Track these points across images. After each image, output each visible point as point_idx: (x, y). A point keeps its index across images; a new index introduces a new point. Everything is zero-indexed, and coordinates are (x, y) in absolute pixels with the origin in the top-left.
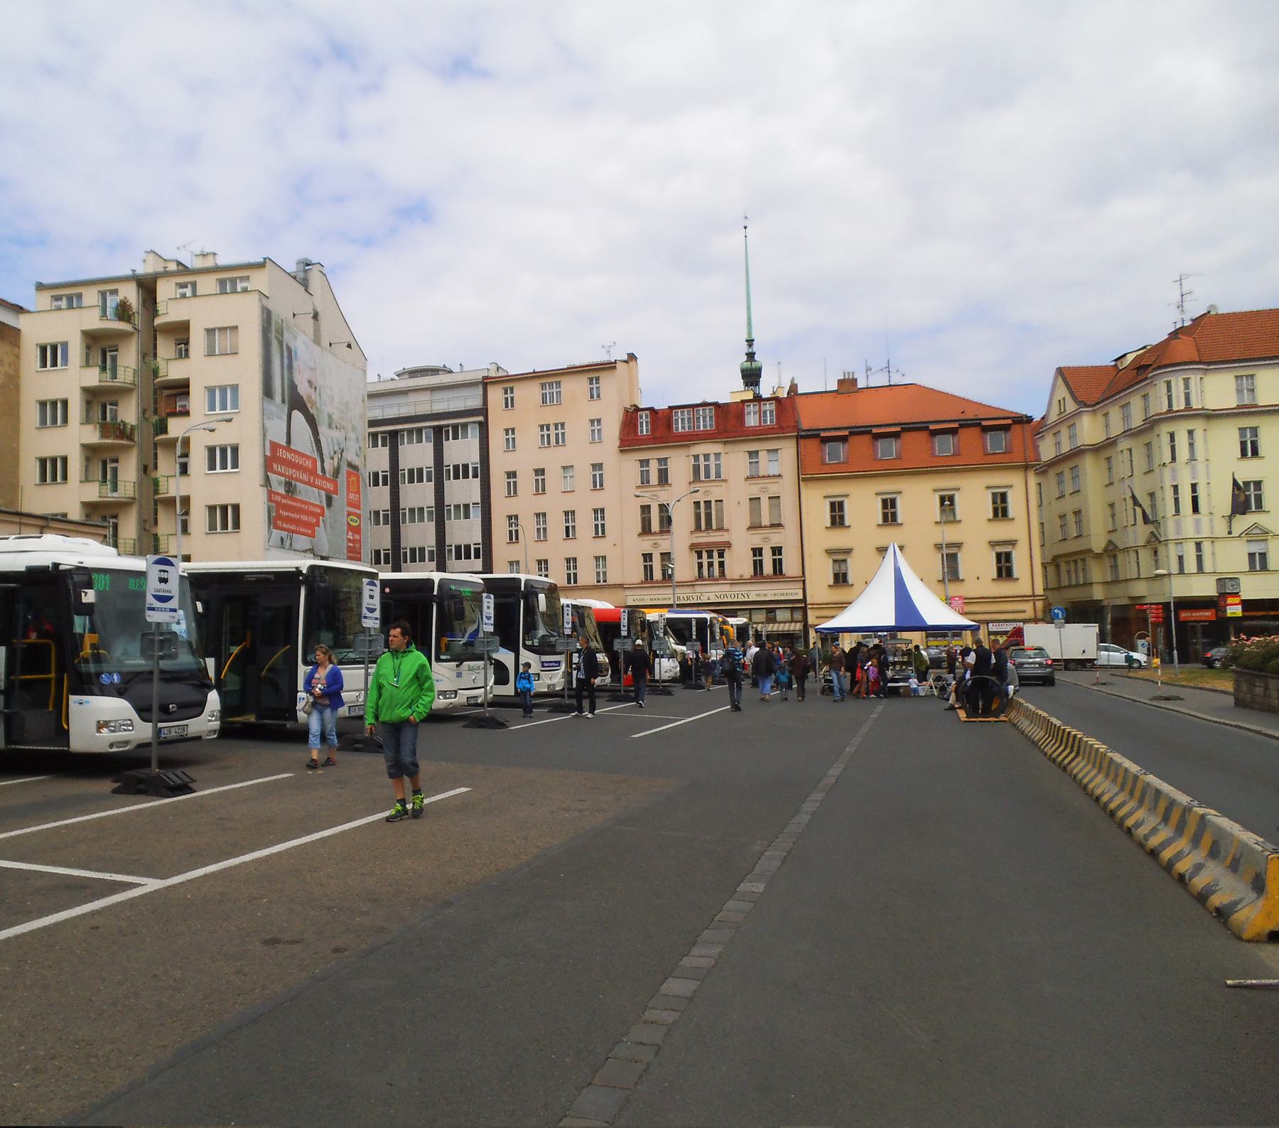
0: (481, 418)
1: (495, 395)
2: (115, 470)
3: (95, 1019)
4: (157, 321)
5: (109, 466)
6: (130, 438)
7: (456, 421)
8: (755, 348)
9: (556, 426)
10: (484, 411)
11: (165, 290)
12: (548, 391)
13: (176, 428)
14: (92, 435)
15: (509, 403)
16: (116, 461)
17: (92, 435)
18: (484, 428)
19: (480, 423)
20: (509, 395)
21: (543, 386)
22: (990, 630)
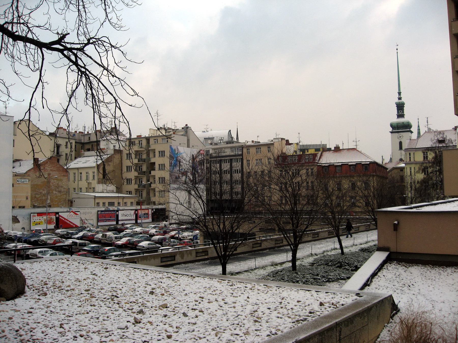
0: (241, 157)
1: (245, 150)
2: (142, 194)
3: (145, 172)
4: (150, 149)
5: (141, 193)
6: (145, 161)
7: (237, 157)
8: (402, 96)
9: (260, 160)
10: (242, 155)
11: (152, 141)
12: (258, 150)
13: (153, 173)
14: (136, 187)
15: (248, 153)
16: (142, 179)
17: (136, 174)
18: (242, 159)
19: (241, 158)
20: (248, 151)
21: (257, 149)
22: (151, 221)
